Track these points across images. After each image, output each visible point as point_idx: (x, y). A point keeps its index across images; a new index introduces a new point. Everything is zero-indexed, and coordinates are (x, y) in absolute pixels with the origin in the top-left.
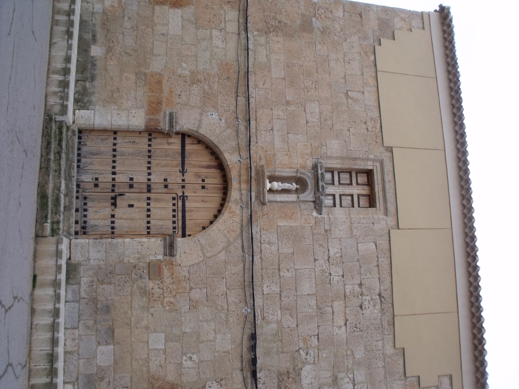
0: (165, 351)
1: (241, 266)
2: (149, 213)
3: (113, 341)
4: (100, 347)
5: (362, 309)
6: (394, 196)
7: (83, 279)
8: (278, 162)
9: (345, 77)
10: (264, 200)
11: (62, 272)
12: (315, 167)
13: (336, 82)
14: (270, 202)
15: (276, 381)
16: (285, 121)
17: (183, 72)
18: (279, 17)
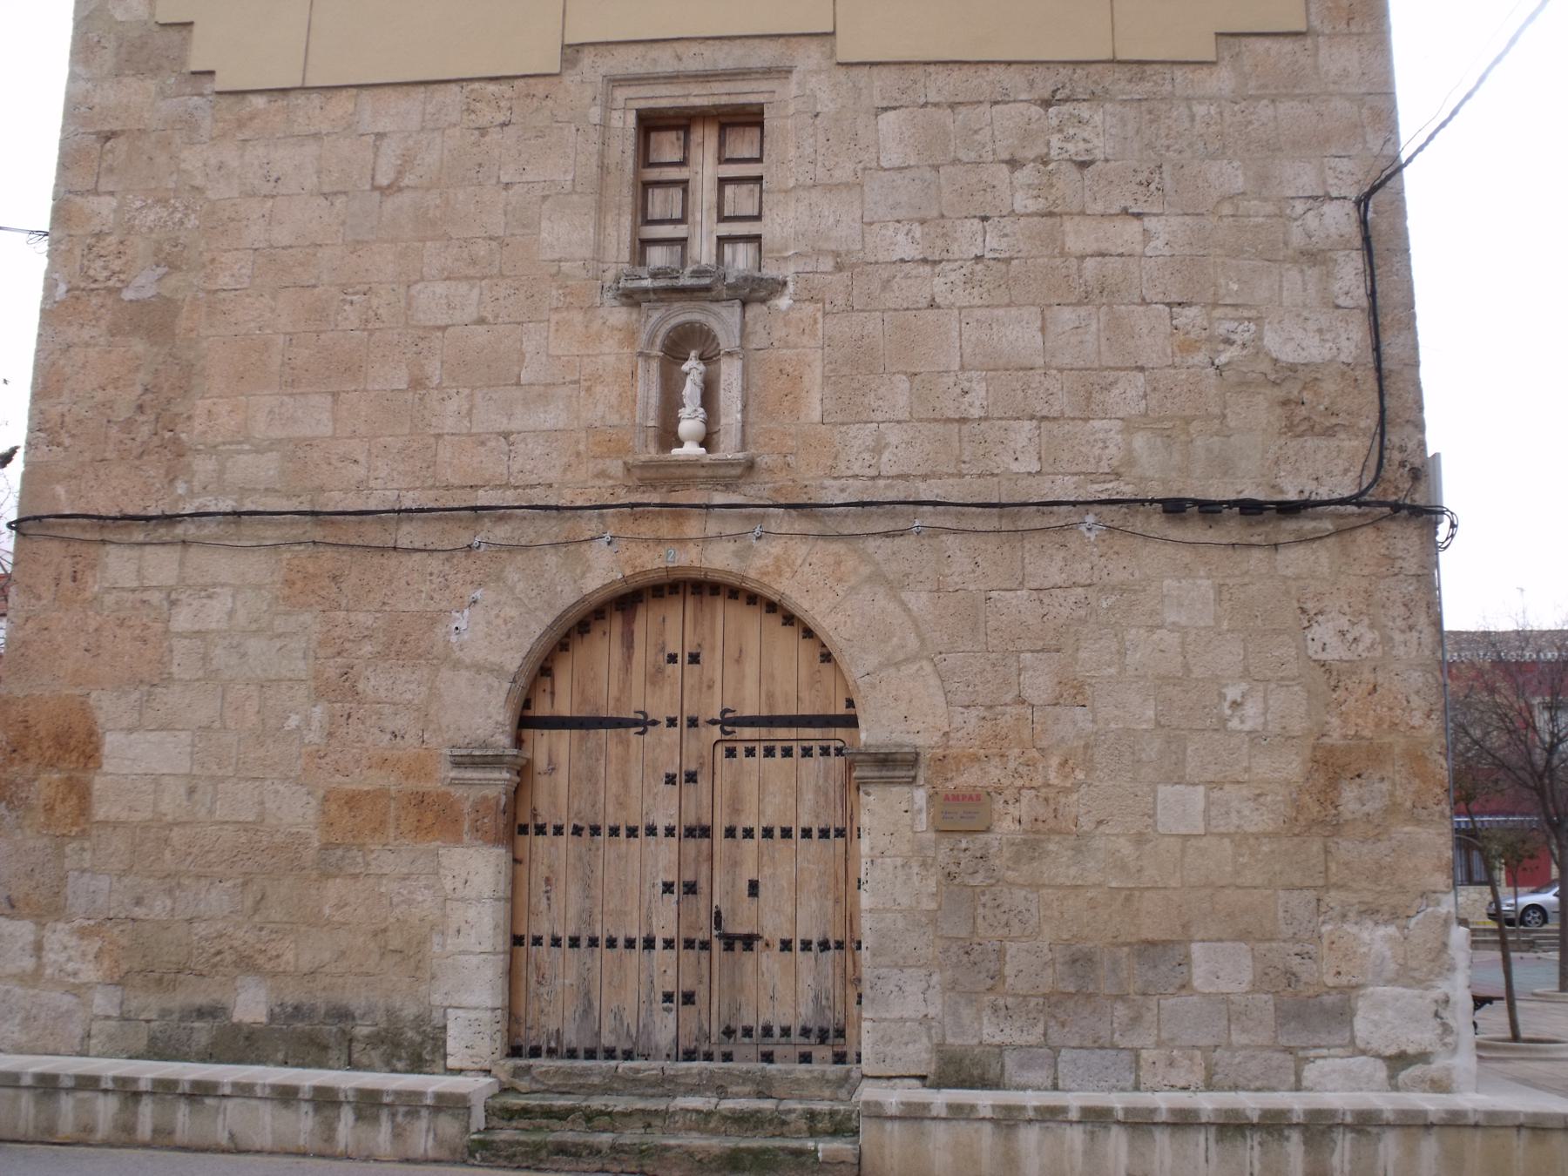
0: (1212, 785)
1: (950, 541)
2: (777, 833)
3: (1179, 942)
4: (1197, 983)
5: (1092, 162)
6: (727, 46)
7: (985, 1037)
8: (614, 419)
9: (326, 196)
10: (739, 464)
11: (972, 1102)
12: (632, 298)
13: (343, 223)
14: (744, 445)
15: (1310, 443)
16: (478, 395)
17: (315, 725)
18: (123, 413)
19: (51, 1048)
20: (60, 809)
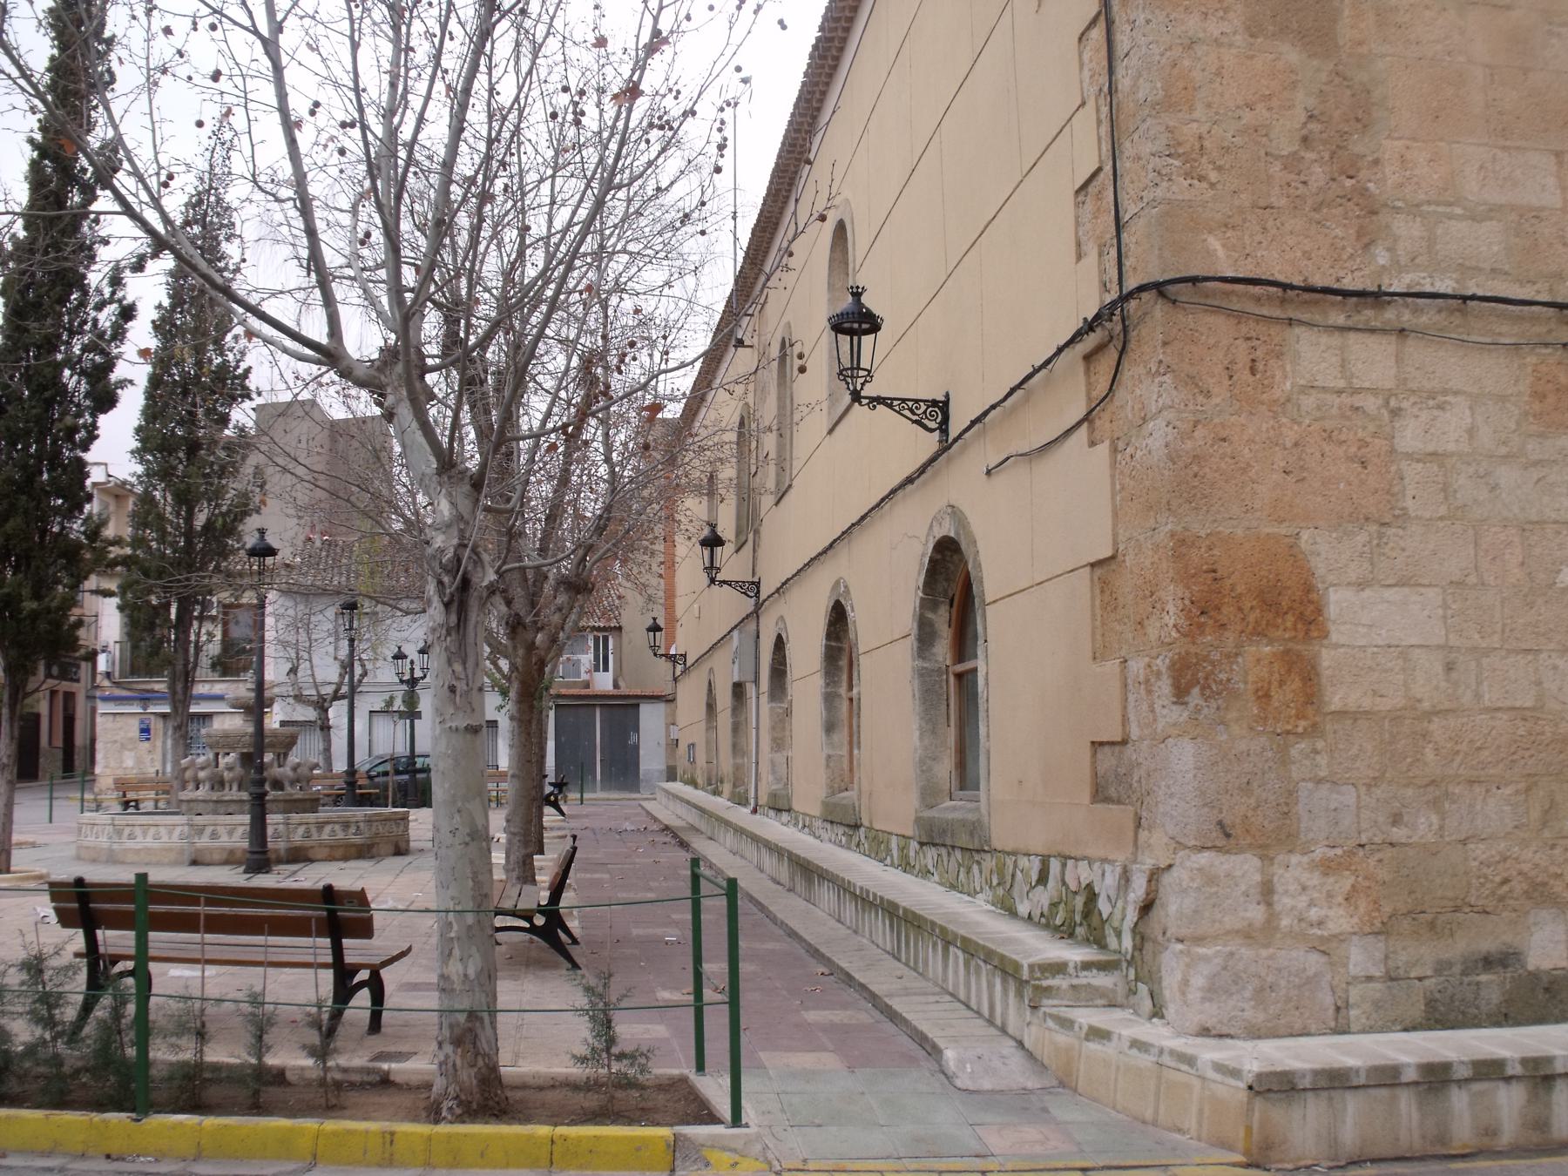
19: (1298, 1026)
20: (1277, 697)
